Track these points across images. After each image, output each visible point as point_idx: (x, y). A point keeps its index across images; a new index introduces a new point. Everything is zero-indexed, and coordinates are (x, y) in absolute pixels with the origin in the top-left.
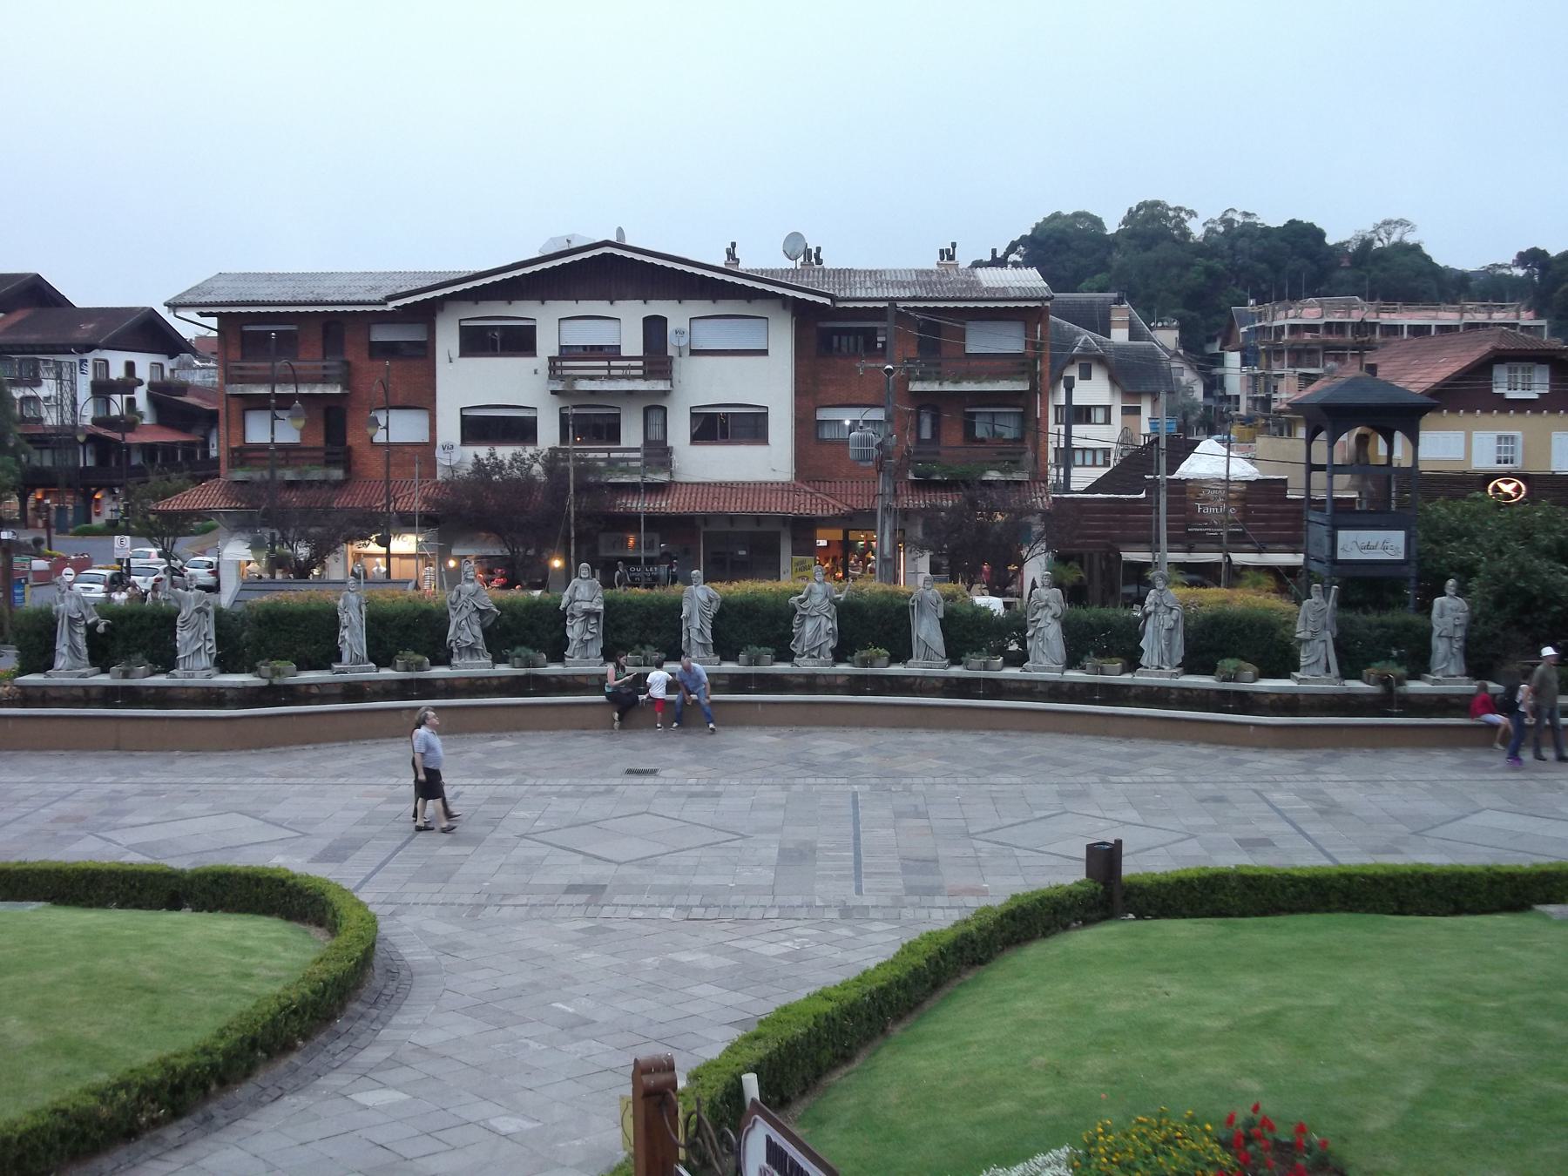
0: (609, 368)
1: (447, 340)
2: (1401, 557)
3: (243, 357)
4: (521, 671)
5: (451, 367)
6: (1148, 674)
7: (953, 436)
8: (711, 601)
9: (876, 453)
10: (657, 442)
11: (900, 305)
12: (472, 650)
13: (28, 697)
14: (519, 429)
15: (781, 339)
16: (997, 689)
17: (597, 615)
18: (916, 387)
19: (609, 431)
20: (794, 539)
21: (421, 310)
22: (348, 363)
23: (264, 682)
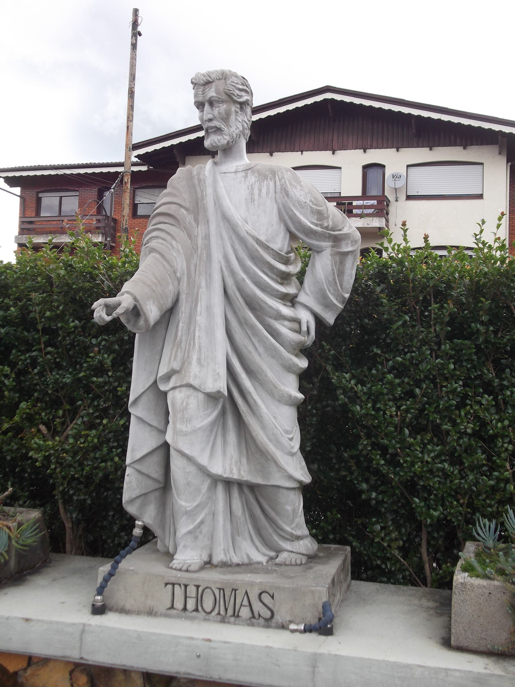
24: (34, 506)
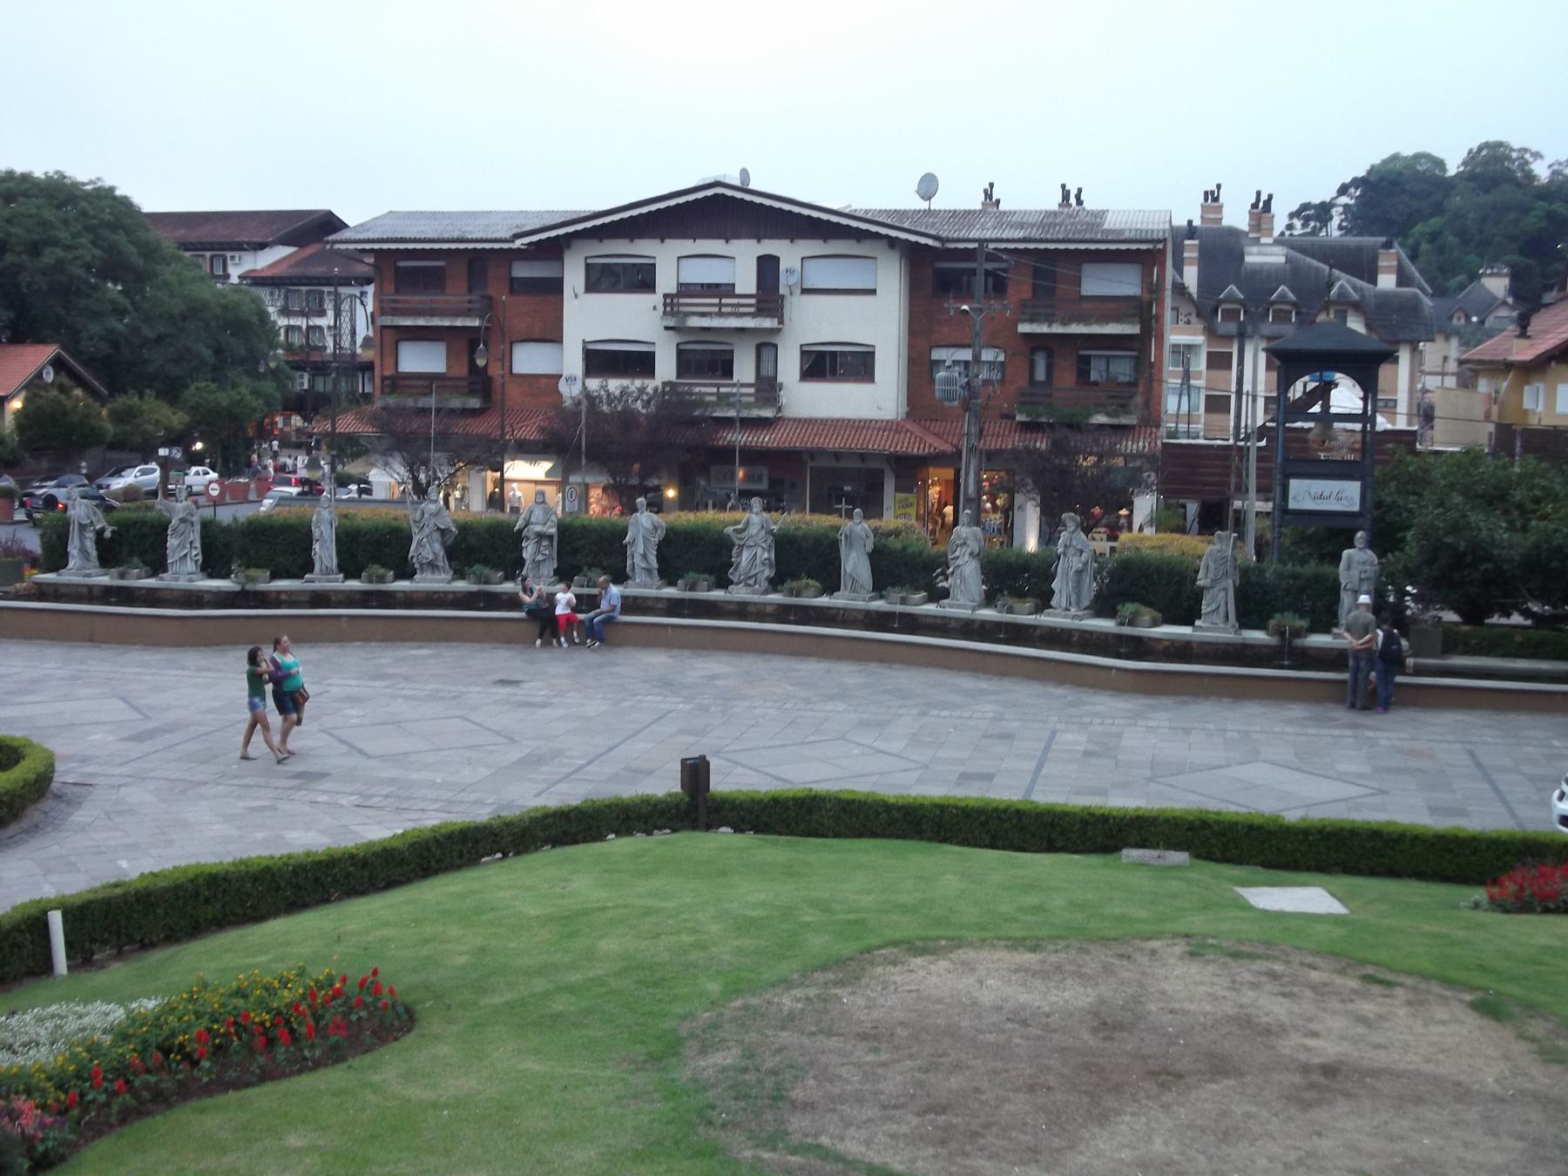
0: (720, 305)
1: (574, 276)
2: (1356, 508)
3: (397, 291)
4: (475, 588)
5: (576, 302)
6: (1054, 616)
7: (1066, 378)
8: (655, 528)
9: (960, 391)
10: (769, 378)
11: (991, 246)
12: (433, 566)
13: (42, 592)
14: (641, 363)
15: (890, 280)
16: (912, 624)
17: (550, 537)
18: (1024, 328)
19: (722, 366)
20: (897, 477)
21: (552, 244)
22: (490, 298)
23: (237, 588)
24: (44, 549)
